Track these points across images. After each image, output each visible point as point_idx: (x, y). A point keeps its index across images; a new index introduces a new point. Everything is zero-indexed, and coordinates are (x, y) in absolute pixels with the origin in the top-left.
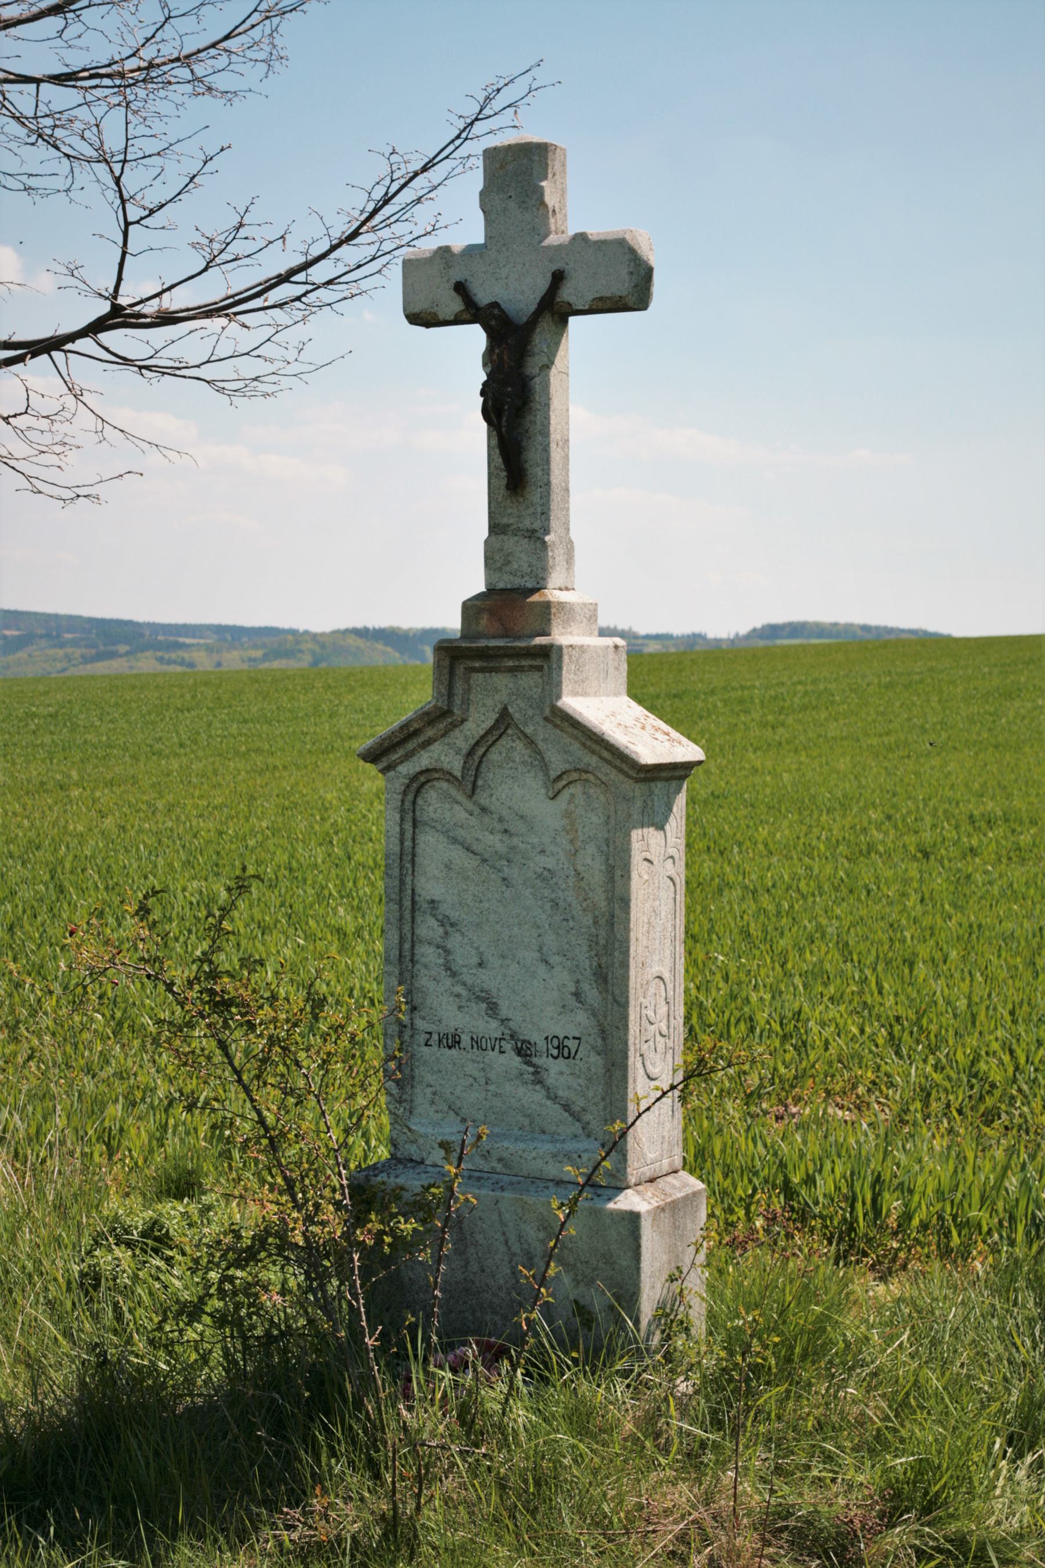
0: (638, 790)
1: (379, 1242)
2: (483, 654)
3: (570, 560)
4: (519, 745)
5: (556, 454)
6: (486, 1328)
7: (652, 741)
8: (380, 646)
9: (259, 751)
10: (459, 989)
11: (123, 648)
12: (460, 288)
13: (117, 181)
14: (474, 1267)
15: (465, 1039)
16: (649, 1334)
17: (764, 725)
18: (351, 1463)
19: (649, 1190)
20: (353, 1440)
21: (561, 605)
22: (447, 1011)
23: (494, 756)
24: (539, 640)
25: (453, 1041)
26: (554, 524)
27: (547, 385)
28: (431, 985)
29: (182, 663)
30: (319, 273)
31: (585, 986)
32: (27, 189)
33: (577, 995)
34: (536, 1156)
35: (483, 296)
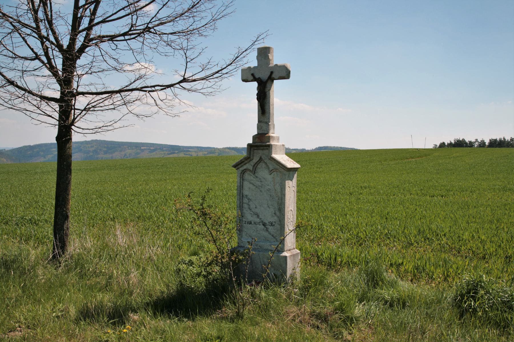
0: (287, 173)
1: (235, 260)
2: (257, 146)
3: (274, 128)
4: (264, 164)
5: (271, 107)
6: (256, 278)
7: (290, 163)
8: (233, 151)
9: (207, 173)
10: (251, 212)
11: (176, 152)
12: (253, 75)
13: (185, 54)
14: (254, 267)
15: (253, 223)
16: (289, 280)
17: (317, 168)
18: (230, 303)
19: (289, 252)
20: (230, 298)
21: (272, 137)
22: (249, 217)
23: (259, 166)
24: (268, 143)
25: (250, 223)
26: (271, 121)
27: (269, 93)
28: (246, 212)
29: (189, 155)
30: (224, 71)
31: (276, 212)
32: (166, 55)
33: (275, 213)
34: (266, 245)
35: (257, 76)
